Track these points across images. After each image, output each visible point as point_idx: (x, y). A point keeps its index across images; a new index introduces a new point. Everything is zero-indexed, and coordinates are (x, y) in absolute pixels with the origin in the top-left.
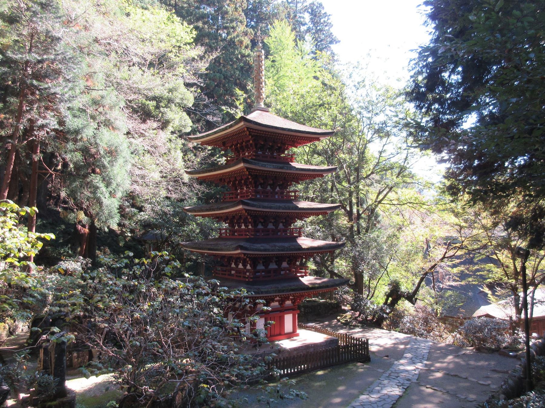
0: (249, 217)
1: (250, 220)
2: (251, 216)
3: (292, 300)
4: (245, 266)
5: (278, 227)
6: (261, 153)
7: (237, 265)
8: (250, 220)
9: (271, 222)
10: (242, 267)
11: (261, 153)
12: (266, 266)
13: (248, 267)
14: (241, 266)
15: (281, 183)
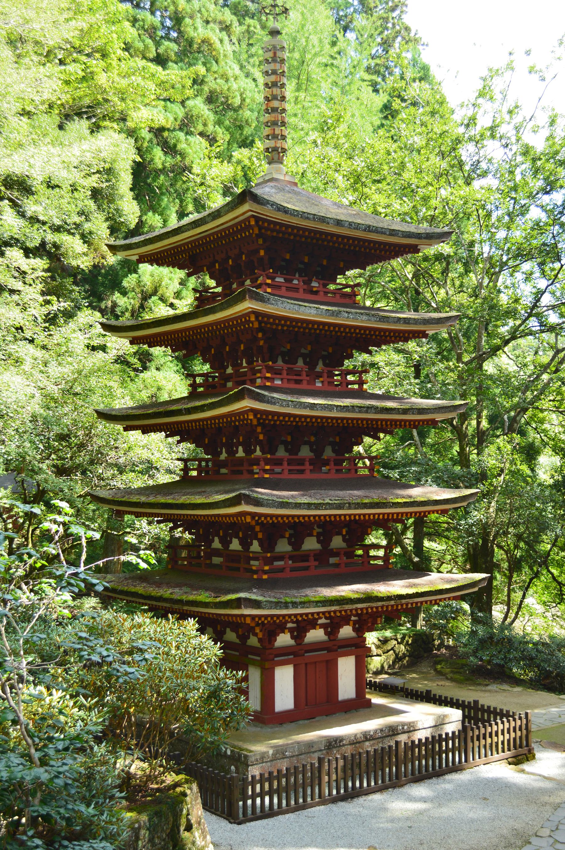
0: (259, 429)
1: (261, 437)
2: (263, 425)
3: (291, 630)
4: (246, 544)
5: (322, 454)
6: (282, 280)
7: (226, 543)
8: (261, 437)
9: (306, 443)
10: (239, 548)
11: (282, 280)
12: (296, 542)
13: (255, 547)
14: (235, 545)
15: (288, 347)
